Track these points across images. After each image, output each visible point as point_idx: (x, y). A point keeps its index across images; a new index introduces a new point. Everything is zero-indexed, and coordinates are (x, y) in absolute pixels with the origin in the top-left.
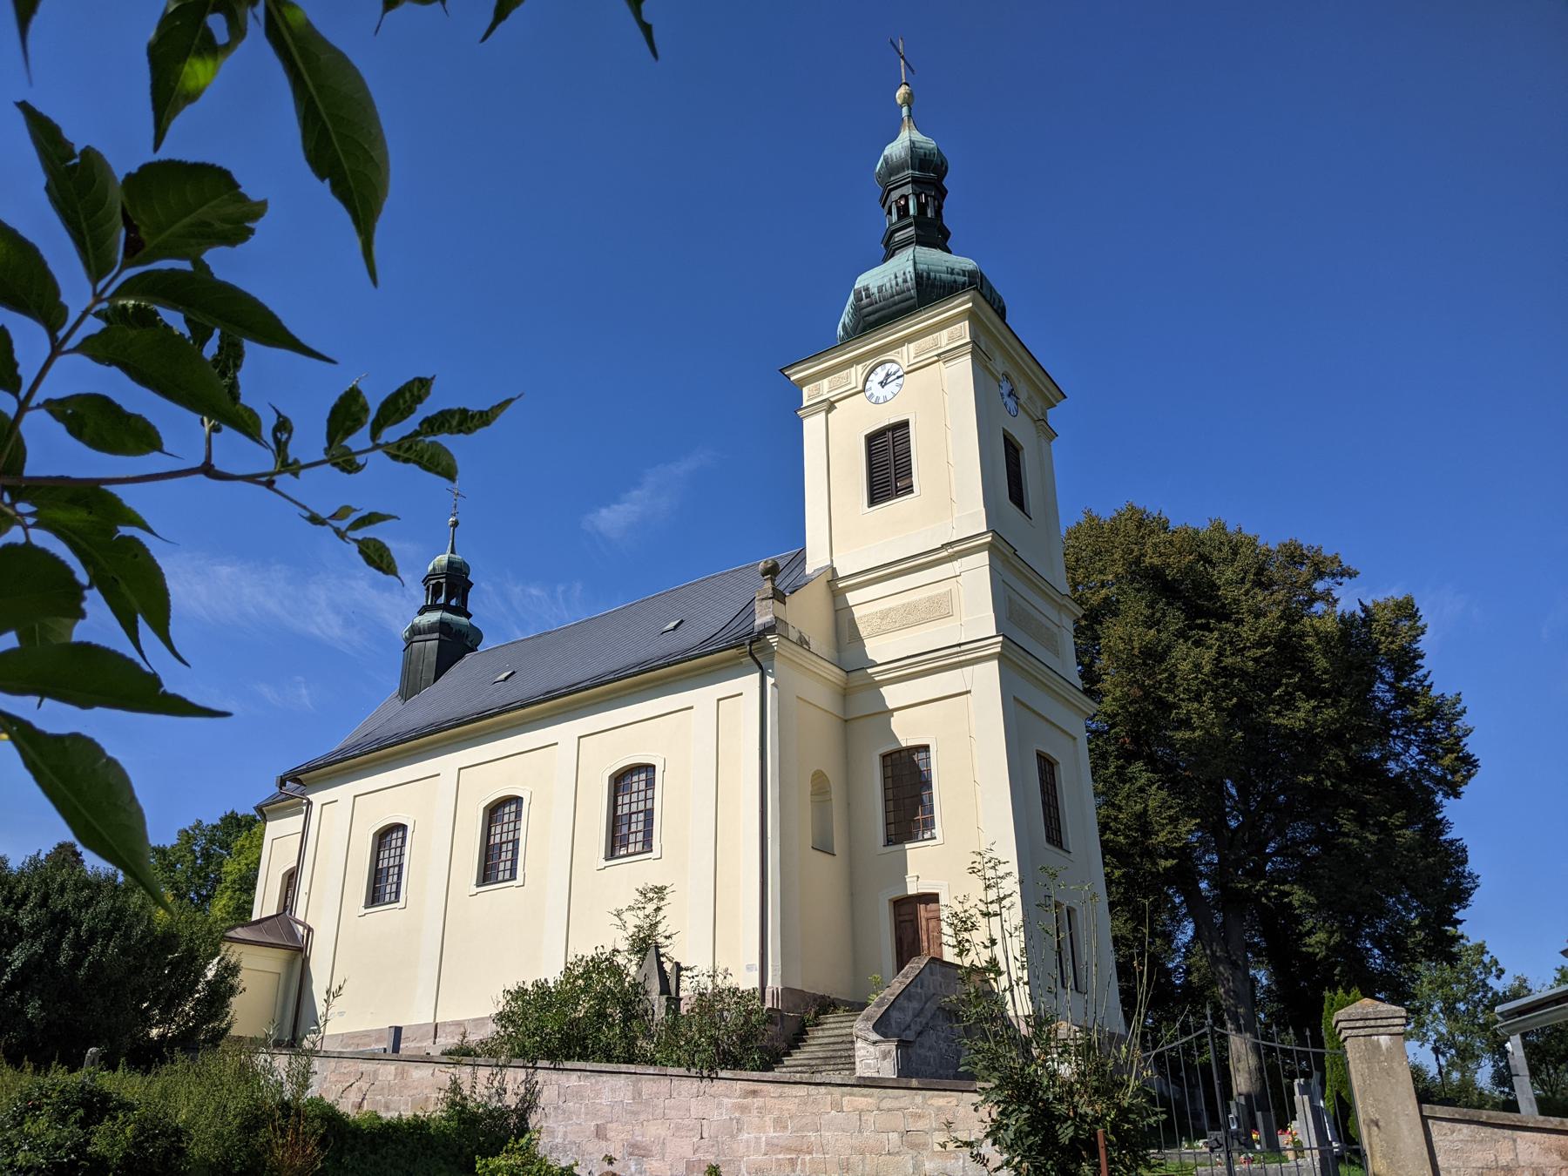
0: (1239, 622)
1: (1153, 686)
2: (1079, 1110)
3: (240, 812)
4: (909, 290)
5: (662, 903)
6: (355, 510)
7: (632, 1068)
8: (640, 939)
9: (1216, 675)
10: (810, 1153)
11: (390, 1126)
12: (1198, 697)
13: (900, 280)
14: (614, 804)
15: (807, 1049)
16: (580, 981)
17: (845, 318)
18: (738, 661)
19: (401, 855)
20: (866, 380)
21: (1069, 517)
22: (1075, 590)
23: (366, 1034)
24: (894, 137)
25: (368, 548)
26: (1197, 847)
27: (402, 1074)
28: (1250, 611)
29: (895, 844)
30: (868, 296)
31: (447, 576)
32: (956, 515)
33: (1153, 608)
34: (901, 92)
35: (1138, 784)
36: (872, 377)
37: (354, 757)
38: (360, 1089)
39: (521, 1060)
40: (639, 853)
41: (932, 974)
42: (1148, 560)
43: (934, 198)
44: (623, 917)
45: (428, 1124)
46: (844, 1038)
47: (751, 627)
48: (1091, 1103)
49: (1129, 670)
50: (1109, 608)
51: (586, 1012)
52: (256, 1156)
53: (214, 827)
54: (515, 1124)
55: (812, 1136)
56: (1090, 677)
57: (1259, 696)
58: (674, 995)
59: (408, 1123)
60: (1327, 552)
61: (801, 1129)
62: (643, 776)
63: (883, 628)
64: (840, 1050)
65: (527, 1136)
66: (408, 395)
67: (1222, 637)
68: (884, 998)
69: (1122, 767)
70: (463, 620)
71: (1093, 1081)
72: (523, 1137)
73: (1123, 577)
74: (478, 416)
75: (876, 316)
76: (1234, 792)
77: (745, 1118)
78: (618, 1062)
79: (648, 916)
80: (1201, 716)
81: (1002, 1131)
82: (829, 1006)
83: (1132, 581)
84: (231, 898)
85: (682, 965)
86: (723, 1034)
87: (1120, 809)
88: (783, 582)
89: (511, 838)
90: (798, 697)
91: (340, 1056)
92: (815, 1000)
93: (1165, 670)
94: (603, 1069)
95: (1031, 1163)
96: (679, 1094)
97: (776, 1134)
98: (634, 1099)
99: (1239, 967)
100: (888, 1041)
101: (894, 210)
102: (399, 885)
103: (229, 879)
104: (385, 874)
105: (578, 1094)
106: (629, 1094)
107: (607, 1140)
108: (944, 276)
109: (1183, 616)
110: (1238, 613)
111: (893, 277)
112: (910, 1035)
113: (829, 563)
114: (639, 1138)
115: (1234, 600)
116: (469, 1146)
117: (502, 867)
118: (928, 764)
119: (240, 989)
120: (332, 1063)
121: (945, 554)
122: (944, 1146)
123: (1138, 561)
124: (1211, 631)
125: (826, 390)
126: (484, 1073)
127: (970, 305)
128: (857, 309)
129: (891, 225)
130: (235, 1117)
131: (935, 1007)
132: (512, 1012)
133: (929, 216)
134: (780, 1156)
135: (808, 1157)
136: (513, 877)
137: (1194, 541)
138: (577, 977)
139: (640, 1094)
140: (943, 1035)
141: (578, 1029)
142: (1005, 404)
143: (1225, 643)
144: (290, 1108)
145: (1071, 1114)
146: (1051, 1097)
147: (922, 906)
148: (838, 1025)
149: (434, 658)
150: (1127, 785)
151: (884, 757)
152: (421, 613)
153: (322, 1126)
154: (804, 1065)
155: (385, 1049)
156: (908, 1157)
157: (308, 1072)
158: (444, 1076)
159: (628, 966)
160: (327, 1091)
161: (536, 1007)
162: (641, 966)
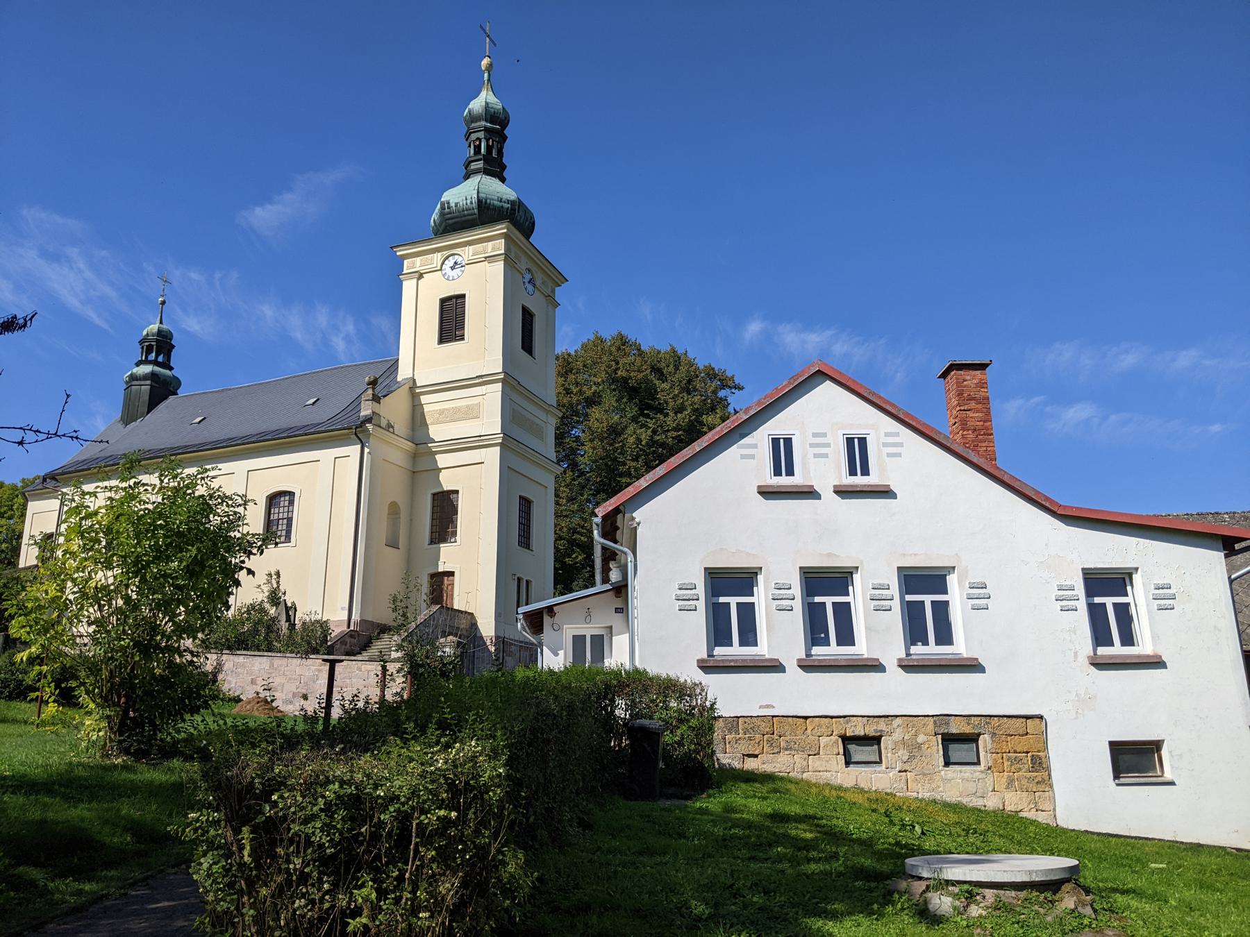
0: (667, 415)
7: (270, 654)
9: (649, 445)
13: (469, 202)
20: (443, 263)
29: (435, 543)
30: (449, 208)
31: (157, 341)
36: (447, 262)
40: (283, 543)
43: (498, 142)
60: (729, 374)
61: (344, 678)
62: (287, 498)
70: (167, 372)
75: (454, 221)
77: (320, 675)
105: (243, 666)
108: (496, 203)
118: (457, 501)
125: (418, 265)
127: (505, 231)
128: (442, 214)
147: (446, 578)
149: (147, 398)
152: (138, 364)
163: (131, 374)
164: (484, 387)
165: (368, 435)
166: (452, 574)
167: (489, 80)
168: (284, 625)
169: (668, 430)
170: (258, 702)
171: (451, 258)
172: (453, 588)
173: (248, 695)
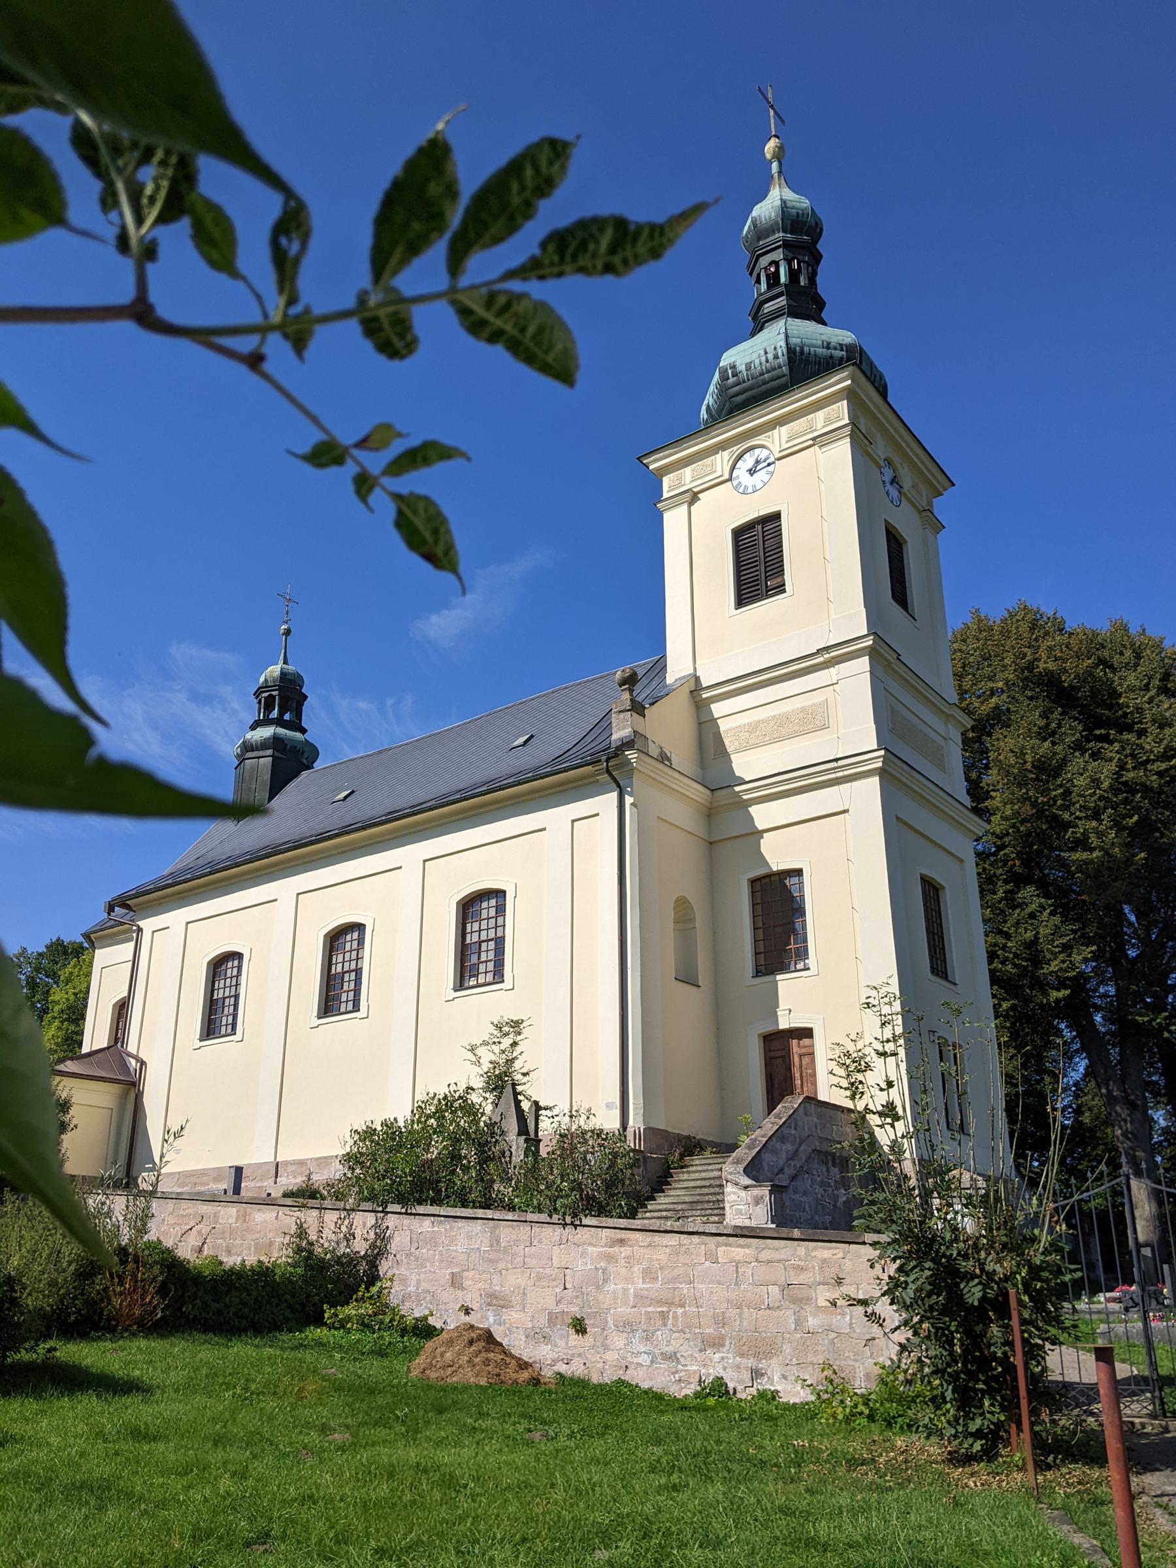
0: (1142, 733)
1: (1048, 802)
2: (987, 1268)
3: (66, 940)
4: (780, 367)
5: (519, 1038)
6: (400, 435)
7: (489, 1213)
8: (496, 1076)
9: (1115, 790)
10: (683, 1306)
11: (233, 1273)
12: (1096, 815)
13: (770, 356)
14: (462, 933)
15: (672, 1193)
16: (432, 1121)
17: (709, 399)
18: (592, 779)
19: (237, 985)
20: (733, 468)
21: (957, 618)
22: (962, 699)
23: (203, 1173)
24: (762, 195)
25: (415, 513)
26: (1090, 977)
27: (244, 1218)
28: (1154, 721)
29: (765, 974)
32: (833, 617)
33: (1048, 718)
34: (771, 145)
35: (1029, 910)
37: (185, 881)
38: (200, 1232)
39: (370, 1203)
41: (806, 1114)
42: (1042, 665)
44: (478, 1052)
45: (273, 1271)
46: (712, 1182)
47: (608, 741)
48: (999, 1261)
49: (1020, 785)
50: (998, 719)
51: (439, 1154)
52: (91, 1304)
53: (40, 954)
54: (365, 1271)
55: (685, 1289)
56: (977, 791)
57: (1162, 814)
58: (532, 1136)
59: (252, 1270)
62: (493, 902)
63: (751, 742)
64: (707, 1194)
65: (379, 1284)
66: (529, 172)
67: (1124, 749)
68: (755, 1140)
69: (1011, 892)
71: (1001, 1237)
72: (374, 1285)
73: (1014, 684)
74: (646, 233)
76: (1133, 918)
77: (612, 1269)
78: (474, 1207)
79: (503, 1052)
80: (1100, 835)
81: (900, 1289)
82: (695, 1147)
83: (1025, 688)
84: (59, 1028)
85: (542, 1104)
86: (587, 1179)
87: (1007, 936)
88: (642, 693)
89: (353, 966)
90: (658, 817)
91: (178, 1197)
92: (679, 1141)
93: (1061, 786)
94: (458, 1214)
95: (932, 1324)
96: (540, 1242)
97: (646, 1286)
98: (491, 1246)
99: (1138, 1110)
100: (760, 1186)
101: (763, 278)
102: (235, 1016)
103: (57, 1008)
104: (220, 1005)
105: (432, 1241)
106: (486, 1241)
107: (463, 1289)
108: (819, 351)
109: (1080, 728)
110: (1140, 722)
111: (762, 352)
112: (783, 1180)
113: (692, 671)
114: (498, 1288)
115: (1137, 709)
116: (317, 1294)
117: (344, 998)
118: (801, 889)
119: (72, 1126)
120: (171, 1204)
121: (821, 659)
122: (834, 1304)
123: (1030, 667)
124: (1111, 742)
125: (688, 481)
126: (331, 1217)
127: (849, 382)
128: (723, 389)
129: (760, 295)
130: (70, 1263)
131: (810, 1149)
132: (360, 1153)
133: (802, 284)
134: (650, 1309)
135: (680, 1311)
136: (356, 1008)
137: (1093, 644)
138: (429, 1117)
139: (498, 1242)
140: (819, 1179)
141: (431, 1172)
142: (887, 493)
143: (1126, 756)
144: (127, 1254)
145: (978, 1271)
146: (955, 1253)
147: (795, 1042)
148: (705, 1168)
150: (1017, 911)
151: (753, 882)
152: (253, 728)
153: (161, 1273)
154: (670, 1210)
155: (225, 1191)
156: (790, 1312)
157: (147, 1216)
158: (288, 1219)
159: (484, 1104)
160: (166, 1233)
161: (385, 1149)
162: (497, 1105)
163: (243, 742)
164: (833, 671)
165: (630, 771)
166: (807, 1033)
167: (780, 172)
168: (516, 1145)
169: (1148, 761)
170: (471, 1342)
171: (747, 456)
172: (813, 1061)
173: (447, 1319)
